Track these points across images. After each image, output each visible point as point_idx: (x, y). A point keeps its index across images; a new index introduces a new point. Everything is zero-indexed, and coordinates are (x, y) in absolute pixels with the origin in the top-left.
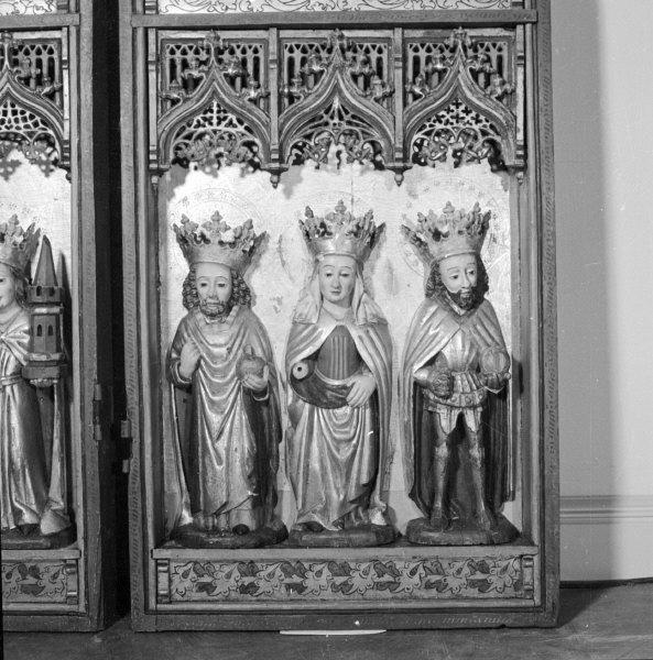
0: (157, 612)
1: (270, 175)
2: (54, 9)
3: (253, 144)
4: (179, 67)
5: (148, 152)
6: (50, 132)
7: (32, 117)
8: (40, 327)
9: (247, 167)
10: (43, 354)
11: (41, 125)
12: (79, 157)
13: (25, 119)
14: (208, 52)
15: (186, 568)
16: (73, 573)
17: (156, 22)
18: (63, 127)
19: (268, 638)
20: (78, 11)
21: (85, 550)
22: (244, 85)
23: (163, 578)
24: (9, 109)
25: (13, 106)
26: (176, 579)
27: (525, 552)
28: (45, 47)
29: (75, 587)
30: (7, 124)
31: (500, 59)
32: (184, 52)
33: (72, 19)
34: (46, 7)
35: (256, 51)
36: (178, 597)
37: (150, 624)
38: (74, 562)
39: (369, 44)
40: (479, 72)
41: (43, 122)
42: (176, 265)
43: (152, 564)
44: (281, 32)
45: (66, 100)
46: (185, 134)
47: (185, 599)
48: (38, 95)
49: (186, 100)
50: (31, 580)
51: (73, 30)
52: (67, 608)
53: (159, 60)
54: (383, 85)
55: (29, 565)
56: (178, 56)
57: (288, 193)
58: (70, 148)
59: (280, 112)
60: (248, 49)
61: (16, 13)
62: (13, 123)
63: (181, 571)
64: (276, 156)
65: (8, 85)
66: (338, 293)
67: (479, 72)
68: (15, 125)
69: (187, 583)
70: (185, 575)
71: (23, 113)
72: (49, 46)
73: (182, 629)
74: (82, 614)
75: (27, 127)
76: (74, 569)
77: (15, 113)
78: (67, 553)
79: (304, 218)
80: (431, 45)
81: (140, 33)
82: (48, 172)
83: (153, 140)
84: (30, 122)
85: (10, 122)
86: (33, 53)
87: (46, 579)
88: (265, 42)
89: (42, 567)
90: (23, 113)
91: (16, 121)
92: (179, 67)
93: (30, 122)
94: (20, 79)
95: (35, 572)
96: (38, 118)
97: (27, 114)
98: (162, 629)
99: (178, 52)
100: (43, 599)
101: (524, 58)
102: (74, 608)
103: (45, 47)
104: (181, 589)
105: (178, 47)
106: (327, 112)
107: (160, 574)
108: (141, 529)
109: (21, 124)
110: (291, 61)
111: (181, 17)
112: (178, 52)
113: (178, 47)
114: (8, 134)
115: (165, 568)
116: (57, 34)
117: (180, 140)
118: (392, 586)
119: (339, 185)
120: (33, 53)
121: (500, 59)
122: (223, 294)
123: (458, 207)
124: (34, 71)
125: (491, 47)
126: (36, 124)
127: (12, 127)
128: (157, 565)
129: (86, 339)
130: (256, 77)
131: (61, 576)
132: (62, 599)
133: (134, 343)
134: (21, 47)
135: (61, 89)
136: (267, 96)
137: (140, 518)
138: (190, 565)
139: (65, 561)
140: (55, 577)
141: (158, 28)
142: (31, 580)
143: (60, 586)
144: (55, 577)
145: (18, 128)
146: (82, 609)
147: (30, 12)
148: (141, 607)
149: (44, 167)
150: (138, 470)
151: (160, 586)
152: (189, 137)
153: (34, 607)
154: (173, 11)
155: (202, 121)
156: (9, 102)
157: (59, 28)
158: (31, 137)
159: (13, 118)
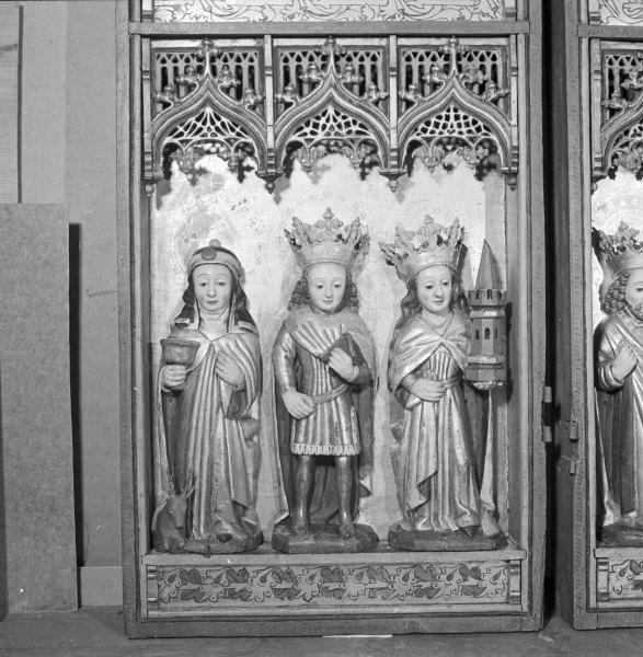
0: (596, 610)
1: (387, 180)
2: (499, 17)
3: (246, 144)
4: (617, 79)
5: (143, 153)
6: (493, 137)
7: (474, 122)
8: (487, 330)
9: (319, 169)
10: (491, 356)
11: (484, 131)
12: (529, 163)
13: (467, 125)
14: (447, 57)
15: (623, 567)
16: (515, 573)
17: (148, 29)
18: (389, 136)
19: (318, 640)
20: (527, 18)
21: (527, 551)
22: (362, 91)
23: (603, 576)
24: (452, 114)
25: (455, 110)
26: (613, 576)
27: (512, 558)
28: (488, 54)
29: (517, 588)
30: (449, 128)
31: (494, 67)
32: (621, 63)
33: (521, 27)
34: (492, 13)
35: (374, 58)
36: (615, 596)
37: (591, 622)
38: (518, 562)
39: (611, 56)
40: (473, 85)
41: (486, 128)
42: (598, 275)
43: (593, 562)
44: (275, 40)
45: (514, 106)
46: (622, 142)
47: (621, 596)
48: (484, 101)
49: (628, 109)
50: (472, 581)
51: (521, 37)
52: (510, 608)
53: (274, 67)
54: (497, 88)
55: (470, 566)
56: (616, 67)
57: (277, 200)
58: (518, 155)
59: (153, 116)
60: (365, 57)
61: (462, 18)
62: (455, 127)
63: (618, 570)
64: (395, 163)
65: (332, 90)
66: (330, 302)
67: (473, 85)
68: (457, 130)
69: (624, 581)
70: (622, 573)
71: (465, 118)
72: (493, 52)
73: (622, 626)
74: (524, 614)
75: (469, 132)
76: (518, 570)
77: (457, 118)
78: (510, 554)
79: (290, 229)
80: (484, 52)
81: (585, 42)
82: (613, 177)
83: (147, 143)
84: (473, 128)
85: (452, 126)
86: (476, 59)
87: (487, 581)
88: (386, 50)
89: (483, 568)
90: (465, 118)
91: (459, 125)
92: (617, 79)
93: (473, 128)
94: (466, 84)
95: (476, 573)
96: (480, 123)
97: (470, 119)
98: (603, 626)
99: (616, 63)
100: (483, 600)
101: (517, 69)
102: (518, 608)
103: (488, 54)
104: (618, 587)
105: (193, 55)
106: (198, 120)
107: (600, 573)
108: (582, 533)
109: (464, 129)
110: (164, 71)
111: (625, 29)
112: (616, 63)
113: (305, 54)
114: (450, 138)
115: (605, 567)
116: (503, 41)
117: (617, 148)
118: (476, 591)
119: (330, 191)
120: (476, 59)
121: (494, 67)
122: (338, 294)
123: (338, 216)
124: (356, 78)
125: (625, 61)
126: (478, 130)
127: (454, 131)
128: (598, 564)
129: (536, 341)
130: (375, 80)
131: (502, 577)
132: (503, 600)
133: (581, 346)
134: (219, 56)
135: (507, 96)
136: (262, 102)
137: (584, 518)
138: (627, 564)
139: (508, 561)
140: (496, 577)
141: (274, 36)
142: (472, 581)
143: (500, 586)
144: (496, 577)
145: (461, 133)
146: (525, 609)
147: (475, 18)
148: (583, 605)
149: (190, 176)
150: (584, 470)
151: (599, 585)
152: (627, 144)
153: (201, 613)
154: (613, 22)
155: (639, 131)
156: (452, 107)
157: (507, 36)
158: (473, 142)
159: (455, 123)
